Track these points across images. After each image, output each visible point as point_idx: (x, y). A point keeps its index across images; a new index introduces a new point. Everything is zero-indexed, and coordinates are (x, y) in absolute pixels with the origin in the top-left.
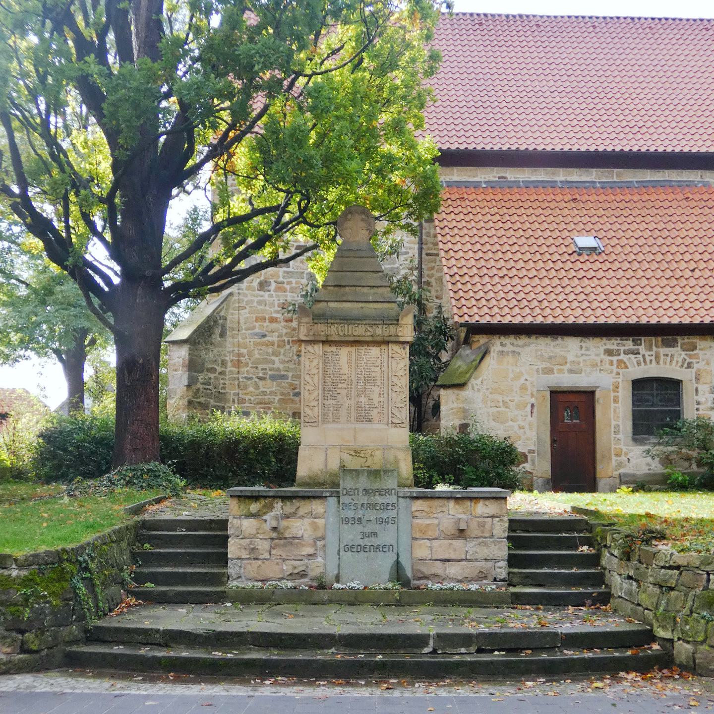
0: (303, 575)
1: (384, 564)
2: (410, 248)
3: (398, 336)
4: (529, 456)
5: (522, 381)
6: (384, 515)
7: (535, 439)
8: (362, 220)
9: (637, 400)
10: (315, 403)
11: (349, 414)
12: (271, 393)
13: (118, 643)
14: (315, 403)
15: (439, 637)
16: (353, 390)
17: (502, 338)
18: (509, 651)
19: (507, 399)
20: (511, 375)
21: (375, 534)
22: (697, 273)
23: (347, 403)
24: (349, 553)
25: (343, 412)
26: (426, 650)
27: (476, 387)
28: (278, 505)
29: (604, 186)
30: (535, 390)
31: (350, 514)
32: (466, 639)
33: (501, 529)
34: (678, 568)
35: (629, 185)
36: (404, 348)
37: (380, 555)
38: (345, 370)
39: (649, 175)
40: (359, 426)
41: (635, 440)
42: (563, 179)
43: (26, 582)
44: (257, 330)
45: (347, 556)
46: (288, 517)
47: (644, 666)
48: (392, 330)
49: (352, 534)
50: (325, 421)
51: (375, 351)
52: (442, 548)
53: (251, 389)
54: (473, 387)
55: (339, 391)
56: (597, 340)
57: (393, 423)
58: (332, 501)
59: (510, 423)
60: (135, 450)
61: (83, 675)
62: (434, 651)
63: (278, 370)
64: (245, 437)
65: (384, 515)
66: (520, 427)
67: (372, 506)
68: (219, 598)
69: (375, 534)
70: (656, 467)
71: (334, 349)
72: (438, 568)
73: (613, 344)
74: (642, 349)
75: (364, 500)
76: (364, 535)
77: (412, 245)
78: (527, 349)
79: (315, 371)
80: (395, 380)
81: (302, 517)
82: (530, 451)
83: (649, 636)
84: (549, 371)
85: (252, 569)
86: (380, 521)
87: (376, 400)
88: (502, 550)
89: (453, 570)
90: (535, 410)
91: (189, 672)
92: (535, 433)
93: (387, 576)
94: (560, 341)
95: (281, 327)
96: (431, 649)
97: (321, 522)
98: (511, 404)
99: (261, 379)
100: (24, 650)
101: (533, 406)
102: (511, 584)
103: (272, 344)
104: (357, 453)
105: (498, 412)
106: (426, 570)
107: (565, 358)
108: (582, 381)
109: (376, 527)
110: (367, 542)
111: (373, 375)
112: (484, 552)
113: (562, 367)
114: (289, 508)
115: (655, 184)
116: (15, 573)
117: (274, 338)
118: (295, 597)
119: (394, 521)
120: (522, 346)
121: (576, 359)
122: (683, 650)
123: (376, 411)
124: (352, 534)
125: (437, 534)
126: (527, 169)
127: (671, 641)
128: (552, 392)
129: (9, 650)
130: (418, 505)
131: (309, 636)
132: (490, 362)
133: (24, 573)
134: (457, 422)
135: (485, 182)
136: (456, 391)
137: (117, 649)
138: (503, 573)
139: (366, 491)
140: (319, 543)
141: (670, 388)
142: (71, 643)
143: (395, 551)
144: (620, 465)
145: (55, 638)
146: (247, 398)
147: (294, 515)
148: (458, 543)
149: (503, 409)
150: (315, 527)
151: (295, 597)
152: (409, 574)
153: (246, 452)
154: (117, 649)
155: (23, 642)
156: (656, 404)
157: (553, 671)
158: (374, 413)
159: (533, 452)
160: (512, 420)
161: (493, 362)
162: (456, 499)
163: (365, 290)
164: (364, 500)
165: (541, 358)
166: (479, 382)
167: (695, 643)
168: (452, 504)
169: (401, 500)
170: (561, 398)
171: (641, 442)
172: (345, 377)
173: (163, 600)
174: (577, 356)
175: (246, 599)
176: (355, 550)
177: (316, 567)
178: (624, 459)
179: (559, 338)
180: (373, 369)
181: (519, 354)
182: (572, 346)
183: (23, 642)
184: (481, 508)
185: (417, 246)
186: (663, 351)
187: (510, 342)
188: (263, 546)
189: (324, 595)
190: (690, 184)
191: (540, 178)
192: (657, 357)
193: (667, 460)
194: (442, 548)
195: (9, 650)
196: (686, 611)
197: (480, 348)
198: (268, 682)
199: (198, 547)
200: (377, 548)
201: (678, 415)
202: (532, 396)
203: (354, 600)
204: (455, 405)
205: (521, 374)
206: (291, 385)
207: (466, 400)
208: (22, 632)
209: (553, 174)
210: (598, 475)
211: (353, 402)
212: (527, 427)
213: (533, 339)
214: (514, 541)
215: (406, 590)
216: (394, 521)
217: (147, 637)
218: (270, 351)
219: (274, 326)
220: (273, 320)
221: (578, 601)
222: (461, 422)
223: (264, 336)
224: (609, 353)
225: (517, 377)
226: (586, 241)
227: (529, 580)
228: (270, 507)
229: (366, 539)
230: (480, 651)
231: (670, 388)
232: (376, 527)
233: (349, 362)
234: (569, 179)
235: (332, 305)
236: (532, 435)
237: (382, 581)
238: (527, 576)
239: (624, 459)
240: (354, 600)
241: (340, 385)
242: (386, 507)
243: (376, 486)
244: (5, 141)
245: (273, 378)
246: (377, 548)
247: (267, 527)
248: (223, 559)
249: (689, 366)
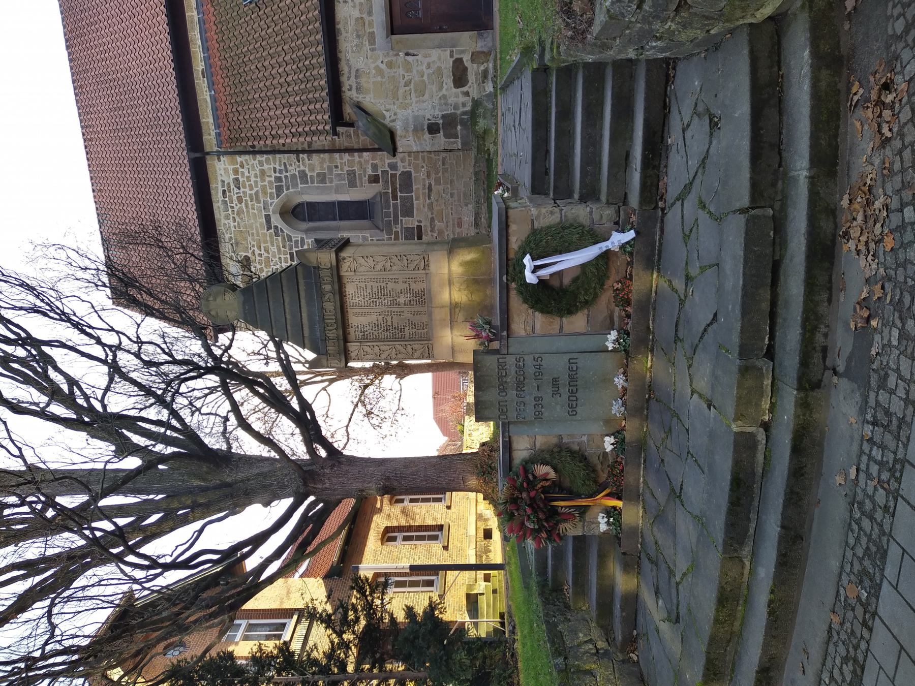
2: (280, 162)
3: (331, 268)
4: (456, 56)
5: (383, 66)
6: (530, 370)
7: (439, 51)
8: (215, 300)
10: (409, 348)
11: (419, 313)
14: (409, 348)
16: (393, 310)
17: (343, 89)
19: (402, 82)
20: (379, 79)
23: (406, 315)
24: (579, 410)
25: (416, 319)
27: (393, 117)
30: (391, 53)
31: (530, 411)
36: (344, 259)
38: (373, 318)
42: (195, 13)
48: (325, 274)
51: (350, 289)
54: (394, 121)
55: (395, 324)
57: (424, 269)
59: (425, 78)
65: (530, 370)
66: (429, 67)
71: (352, 330)
77: (277, 159)
78: (352, 62)
79: (376, 349)
80: (379, 267)
82: (451, 56)
84: (372, 37)
87: (401, 286)
90: (411, 51)
92: (434, 51)
94: (340, 26)
96: (761, 430)
98: (407, 78)
101: (407, 54)
105: (416, 91)
107: (357, 19)
111: (375, 290)
113: (367, 23)
120: (350, 67)
121: (358, 8)
123: (413, 286)
126: (192, 50)
128: (392, 34)
132: (370, 101)
134: (427, 136)
135: (210, 91)
136: (398, 139)
143: (575, 355)
149: (412, 86)
158: (416, 287)
159: (452, 52)
160: (422, 76)
161: (368, 99)
165: (359, 46)
166: (387, 114)
169: (511, 350)
170: (398, 22)
172: (380, 318)
174: (354, 7)
176: (574, 403)
179: (338, 27)
180: (369, 290)
181: (357, 70)
185: (278, 156)
187: (348, 82)
191: (198, 36)
197: (355, 113)
199: (601, 104)
202: (397, 55)
204: (411, 138)
205: (377, 68)
207: (406, 129)
209: (192, 22)
211: (405, 310)
212: (427, 60)
213: (342, 56)
222: (427, 133)
225: (380, 72)
229: (561, 391)
233: (364, 314)
234: (194, 6)
236: (435, 54)
241: (389, 323)
242: (520, 368)
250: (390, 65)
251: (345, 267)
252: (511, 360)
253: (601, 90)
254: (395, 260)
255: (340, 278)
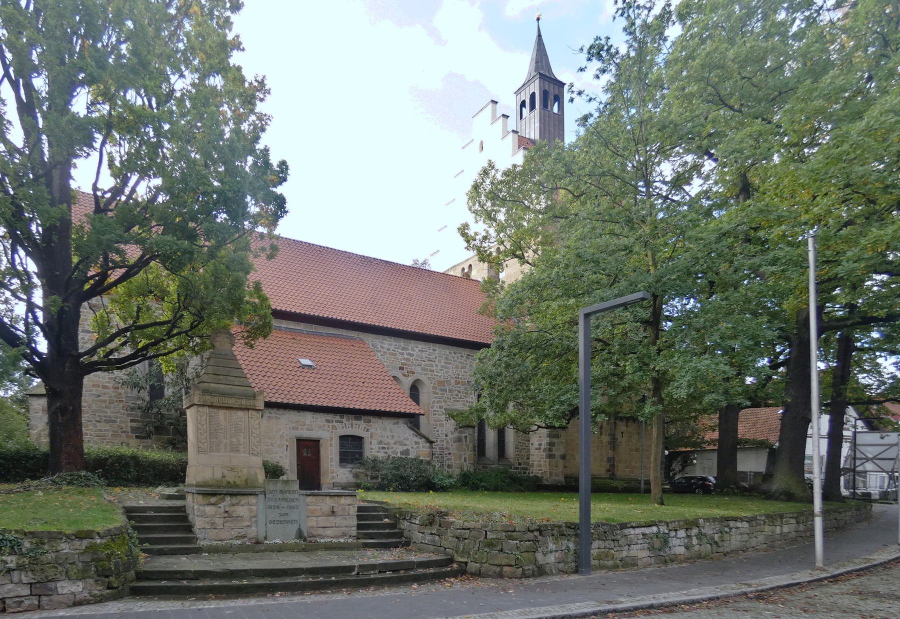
0: (244, 537)
1: (293, 530)
6: (292, 504)
9: (341, 446)
12: (106, 430)
13: (162, 580)
15: (360, 566)
18: (394, 571)
21: (287, 514)
22: (366, 385)
26: (354, 573)
28: (228, 498)
29: (308, 333)
31: (273, 504)
32: (373, 567)
33: (353, 511)
34: (469, 529)
35: (321, 335)
37: (290, 525)
39: (331, 331)
40: (232, 454)
41: (341, 466)
43: (107, 546)
44: (94, 392)
45: (270, 526)
46: (234, 505)
47: (454, 574)
49: (273, 515)
50: (211, 450)
51: (240, 413)
52: (322, 521)
53: (91, 427)
56: (321, 414)
58: (261, 496)
60: (69, 463)
61: (149, 600)
62: (358, 574)
63: (110, 417)
64: (111, 456)
65: (292, 504)
67: (286, 500)
68: (198, 551)
69: (287, 514)
70: (351, 479)
71: (215, 410)
72: (320, 531)
73: (330, 417)
74: (344, 420)
75: (280, 496)
76: (281, 515)
81: (243, 505)
83: (451, 561)
84: (296, 429)
85: (213, 533)
86: (290, 507)
88: (354, 522)
89: (329, 532)
91: (222, 593)
93: (294, 536)
94: (302, 413)
95: (111, 391)
97: (254, 508)
99: (99, 422)
100: (109, 587)
102: (358, 538)
103: (105, 401)
104: (232, 469)
106: (314, 533)
108: (313, 435)
109: (288, 511)
110: (282, 518)
112: (344, 523)
114: (235, 500)
115: (335, 336)
116: (99, 541)
117: (106, 398)
118: (243, 549)
119: (297, 507)
122: (473, 567)
124: (273, 515)
125: (320, 514)
127: (466, 563)
129: (101, 588)
130: (310, 499)
131: (289, 569)
133: (104, 541)
137: (163, 583)
138: (354, 533)
139: (281, 492)
140: (253, 520)
141: (358, 441)
142: (132, 581)
144: (333, 478)
145: (126, 579)
146: (89, 432)
147: (238, 504)
148: (332, 518)
150: (251, 511)
151: (243, 549)
152: (306, 535)
153: (113, 464)
154: (163, 583)
155: (109, 583)
156: (351, 449)
157: (420, 579)
158: (241, 448)
162: (330, 496)
163: (232, 378)
164: (280, 496)
167: (481, 563)
168: (328, 498)
171: (344, 467)
173: (161, 553)
175: (213, 550)
177: (252, 532)
178: (335, 475)
182: (308, 417)
183: (109, 583)
184: (343, 501)
186: (355, 422)
188: (219, 521)
189: (262, 547)
190: (352, 338)
192: (352, 425)
193: (356, 476)
194: (322, 521)
195: (101, 588)
196: (476, 548)
198: (277, 595)
199: (165, 522)
200: (288, 522)
201: (361, 454)
203: (279, 549)
206: (119, 426)
208: (107, 577)
210: (322, 482)
213: (287, 411)
214: (359, 517)
215: (306, 543)
216: (297, 507)
217: (182, 575)
218: (104, 405)
219: (106, 391)
220: (104, 387)
221: (396, 546)
223: (99, 396)
224: (328, 421)
226: (305, 362)
227: (371, 536)
228: (224, 500)
230: (380, 572)
231: (358, 441)
232: (288, 511)
235: (212, 385)
237: (292, 540)
238: (366, 534)
239: (335, 475)
240: (279, 549)
242: (293, 500)
243: (287, 488)
244: (2, 248)
245: (107, 422)
246: (288, 522)
247: (222, 510)
248: (189, 528)
249: (368, 430)
250: (282, 436)
251: (254, 413)
252: (297, 496)
253: (160, 521)
254: (258, 439)
255: (248, 409)
